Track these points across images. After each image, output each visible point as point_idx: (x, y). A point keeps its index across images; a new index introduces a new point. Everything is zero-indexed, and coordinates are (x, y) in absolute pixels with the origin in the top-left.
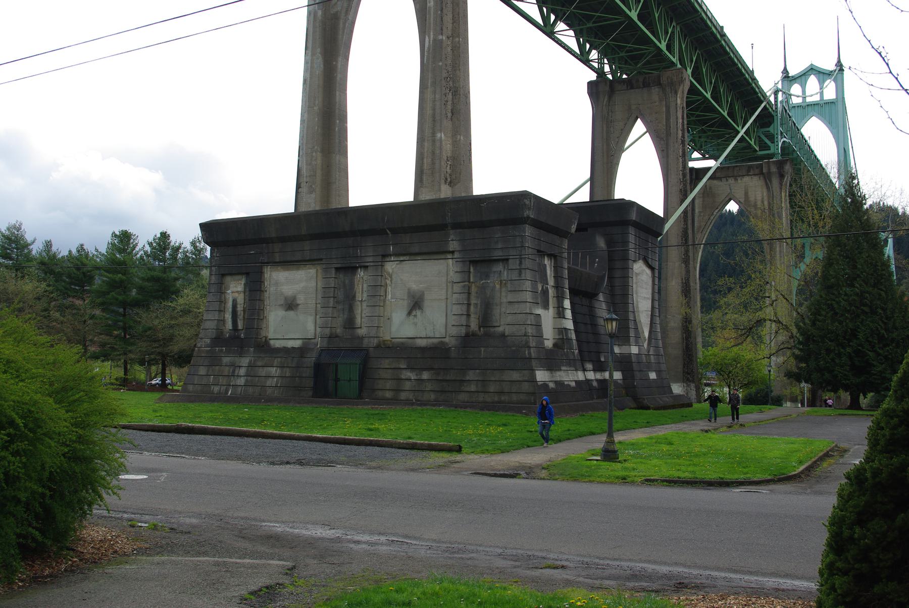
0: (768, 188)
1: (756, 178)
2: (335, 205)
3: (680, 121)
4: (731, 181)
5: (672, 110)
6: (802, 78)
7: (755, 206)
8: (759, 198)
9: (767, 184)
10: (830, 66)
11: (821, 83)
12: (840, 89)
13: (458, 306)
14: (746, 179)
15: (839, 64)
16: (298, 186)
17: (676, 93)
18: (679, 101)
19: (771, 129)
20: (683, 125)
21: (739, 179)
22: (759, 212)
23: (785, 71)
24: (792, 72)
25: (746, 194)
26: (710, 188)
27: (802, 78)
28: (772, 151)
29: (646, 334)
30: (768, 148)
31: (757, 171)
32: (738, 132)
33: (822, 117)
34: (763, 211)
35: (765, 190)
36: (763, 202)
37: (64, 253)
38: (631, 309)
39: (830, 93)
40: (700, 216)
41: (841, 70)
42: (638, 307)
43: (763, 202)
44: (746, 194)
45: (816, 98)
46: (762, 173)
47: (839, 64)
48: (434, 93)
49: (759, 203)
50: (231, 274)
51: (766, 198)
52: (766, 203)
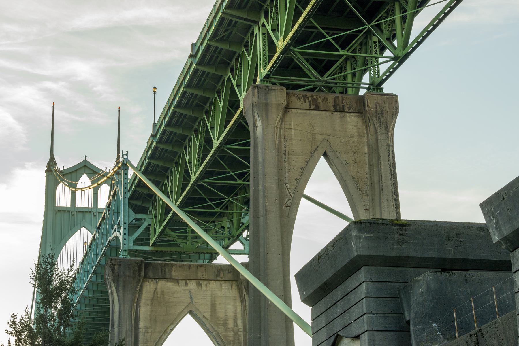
1: (226, 286)
2: (388, 215)
4: (192, 285)
6: (71, 176)
7: (225, 325)
8: (231, 315)
11: (73, 186)
13: (371, 285)
14: (214, 285)
21: (203, 283)
22: (231, 335)
23: (52, 163)
24: (62, 165)
25: (213, 306)
26: (163, 293)
27: (71, 176)
34: (236, 334)
35: (239, 304)
36: (235, 321)
40: (146, 332)
43: (235, 321)
44: (213, 306)
45: (67, 204)
49: (231, 322)
51: (239, 316)
52: (240, 322)
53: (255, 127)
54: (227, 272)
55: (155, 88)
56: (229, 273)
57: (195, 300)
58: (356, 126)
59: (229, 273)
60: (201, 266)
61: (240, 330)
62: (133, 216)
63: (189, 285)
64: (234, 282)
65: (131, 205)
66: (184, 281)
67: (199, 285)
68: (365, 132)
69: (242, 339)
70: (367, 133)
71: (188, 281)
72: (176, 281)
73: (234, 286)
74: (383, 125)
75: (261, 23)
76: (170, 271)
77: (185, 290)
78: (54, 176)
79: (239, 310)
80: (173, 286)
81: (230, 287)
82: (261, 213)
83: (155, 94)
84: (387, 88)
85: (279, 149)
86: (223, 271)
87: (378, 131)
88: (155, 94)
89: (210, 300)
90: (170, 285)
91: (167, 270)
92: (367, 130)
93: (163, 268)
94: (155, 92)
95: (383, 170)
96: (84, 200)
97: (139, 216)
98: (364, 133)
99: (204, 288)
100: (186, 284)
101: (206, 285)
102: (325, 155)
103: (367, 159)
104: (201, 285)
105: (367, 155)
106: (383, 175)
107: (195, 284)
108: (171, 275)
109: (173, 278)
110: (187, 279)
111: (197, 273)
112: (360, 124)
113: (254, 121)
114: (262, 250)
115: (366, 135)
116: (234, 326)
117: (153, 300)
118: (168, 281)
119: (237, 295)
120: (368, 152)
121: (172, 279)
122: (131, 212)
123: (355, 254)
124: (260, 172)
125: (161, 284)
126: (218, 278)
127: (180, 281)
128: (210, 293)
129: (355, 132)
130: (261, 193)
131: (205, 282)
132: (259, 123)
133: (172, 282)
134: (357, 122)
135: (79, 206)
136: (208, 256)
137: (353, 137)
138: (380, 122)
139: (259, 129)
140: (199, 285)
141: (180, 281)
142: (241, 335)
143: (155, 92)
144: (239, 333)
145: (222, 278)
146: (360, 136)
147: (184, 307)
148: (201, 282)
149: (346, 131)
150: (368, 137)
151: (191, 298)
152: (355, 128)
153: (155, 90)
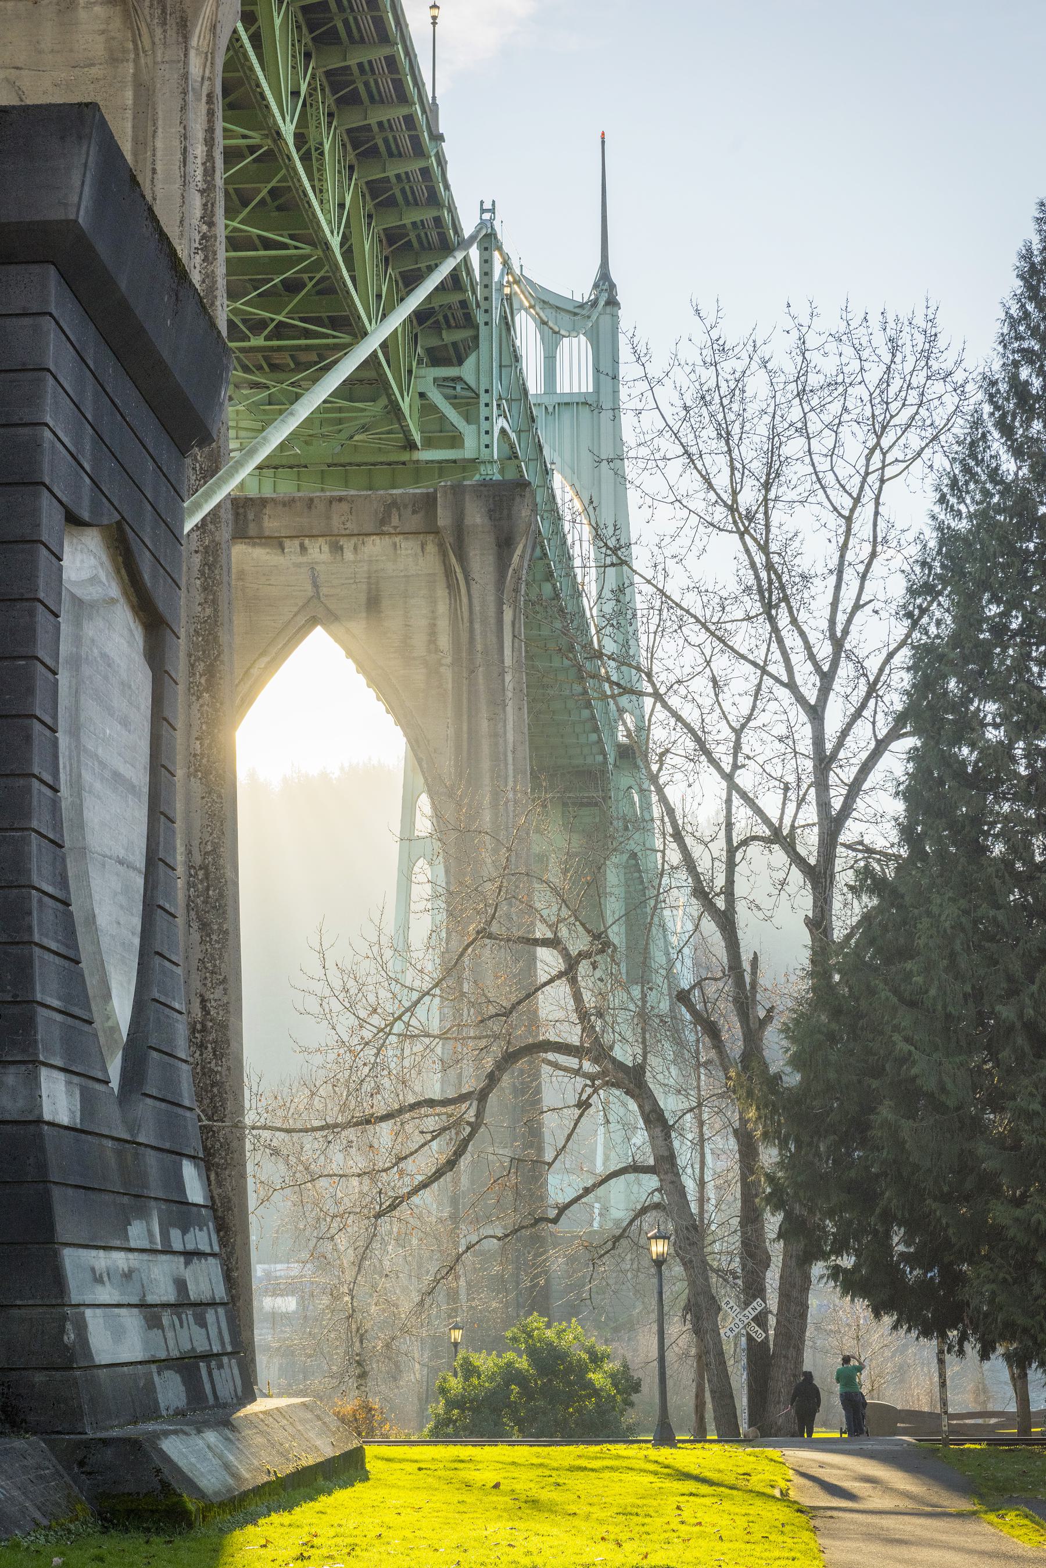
0: (452, 586)
1: (408, 547)
2: (66, 1226)
3: (199, 150)
4: (319, 552)
5: (165, 104)
9: (448, 572)
12: (607, 371)
14: (376, 547)
15: (605, 282)
17: (184, 27)
18: (195, 66)
19: (467, 371)
20: (209, 172)
21: (348, 545)
28: (469, 449)
29: (121, 1007)
30: (455, 440)
31: (415, 521)
35: (441, 592)
38: (39, 821)
41: (612, 303)
42: (80, 825)
46: (433, 530)
47: (605, 282)
48: (112, 1427)
54: (410, 510)
55: (435, 6)
56: (414, 512)
57: (324, 590)
58: (103, 32)
59: (414, 512)
60: (340, 499)
61: (444, 661)
63: (310, 551)
64: (431, 537)
66: (297, 542)
67: (337, 549)
68: (131, 46)
69: (450, 686)
70: (136, 48)
71: (307, 541)
72: (277, 543)
73: (431, 548)
74: (171, 21)
76: (258, 519)
77: (298, 565)
80: (268, 557)
81: (419, 551)
83: (434, 24)
86: (398, 509)
87: (157, 40)
88: (434, 24)
89: (364, 587)
91: (251, 516)
92: (134, 42)
93: (241, 511)
94: (434, 18)
95: (159, 154)
98: (125, 51)
99: (349, 555)
100: (303, 548)
101: (355, 548)
103: (129, 125)
104: (341, 548)
105: (129, 114)
106: (159, 168)
107: (326, 548)
108: (261, 527)
109: (267, 534)
110: (302, 535)
111: (329, 518)
112: (117, 23)
115: (132, 56)
116: (429, 651)
118: (254, 545)
119: (439, 569)
120: (135, 104)
126: (385, 529)
127: (287, 543)
128: (365, 568)
129: (98, 48)
131: (354, 540)
133: (261, 545)
134: (108, 20)
135: (567, 390)
137: (93, 65)
138: (164, 11)
140: (337, 549)
141: (287, 543)
143: (434, 18)
144: (442, 669)
145: (395, 528)
146: (114, 60)
147: (296, 609)
148: (342, 541)
149: (71, 51)
150: (136, 61)
151: (316, 585)
152: (101, 39)
153: (435, 12)
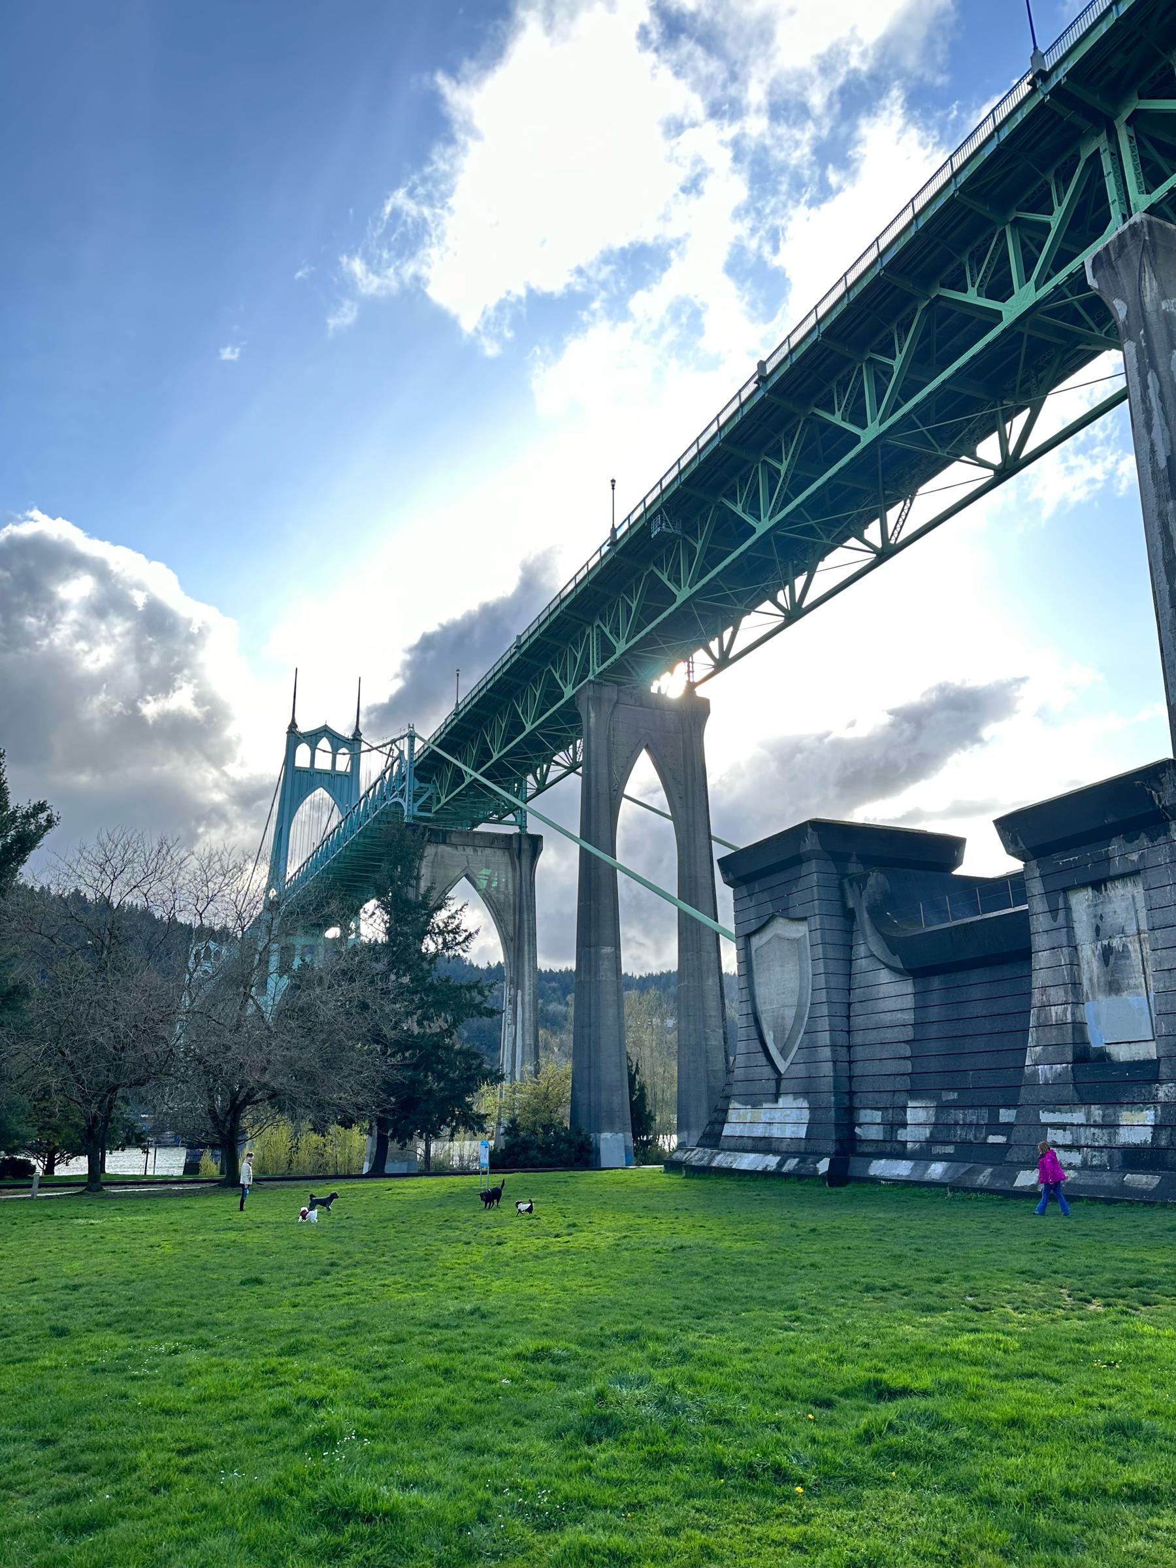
0: (514, 869)
1: (499, 853)
4: (469, 851)
9: (513, 863)
10: (348, 734)
14: (488, 851)
15: (357, 733)
16: (1156, 606)
21: (479, 850)
22: (502, 897)
23: (293, 725)
24: (303, 728)
26: (442, 856)
27: (312, 739)
32: (476, 780)
33: (331, 790)
34: (506, 896)
35: (510, 870)
36: (507, 886)
37: (566, 339)
39: (343, 763)
43: (507, 886)
47: (357, 733)
50: (720, 968)
51: (510, 880)
52: (510, 886)
53: (589, 718)
62: (417, 784)
65: (416, 775)
67: (475, 851)
72: (455, 846)
75: (595, 625)
78: (294, 737)
79: (510, 875)
82: (593, 795)
84: (700, 692)
85: (608, 738)
90: (449, 849)
96: (323, 762)
97: (423, 785)
102: (647, 747)
113: (588, 713)
114: (593, 827)
117: (433, 862)
121: (451, 845)
122: (416, 781)
123: (809, 848)
124: (593, 758)
125: (442, 848)
130: (593, 778)
132: (592, 715)
136: (470, 823)
139: (592, 720)
142: (511, 898)
